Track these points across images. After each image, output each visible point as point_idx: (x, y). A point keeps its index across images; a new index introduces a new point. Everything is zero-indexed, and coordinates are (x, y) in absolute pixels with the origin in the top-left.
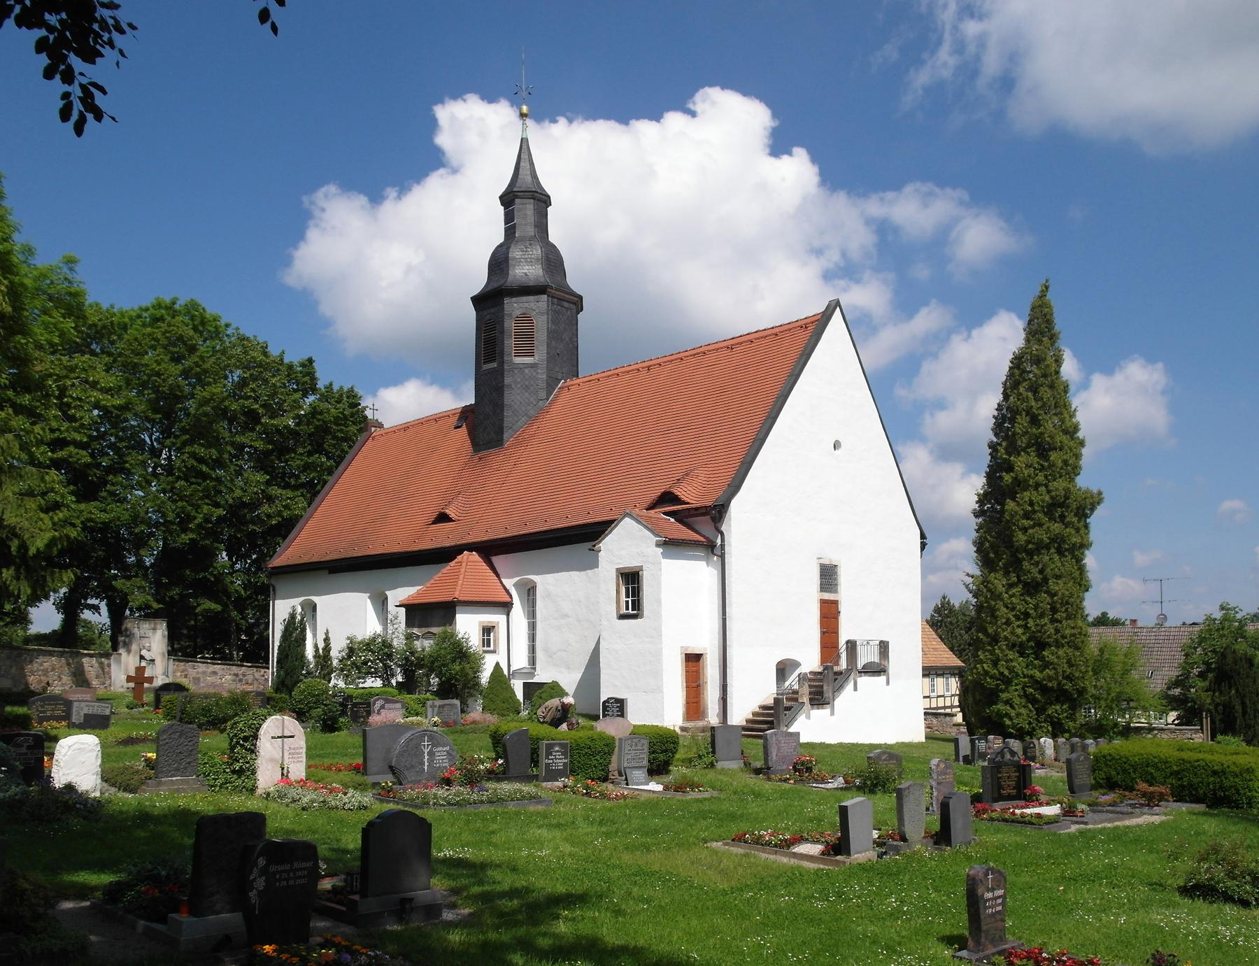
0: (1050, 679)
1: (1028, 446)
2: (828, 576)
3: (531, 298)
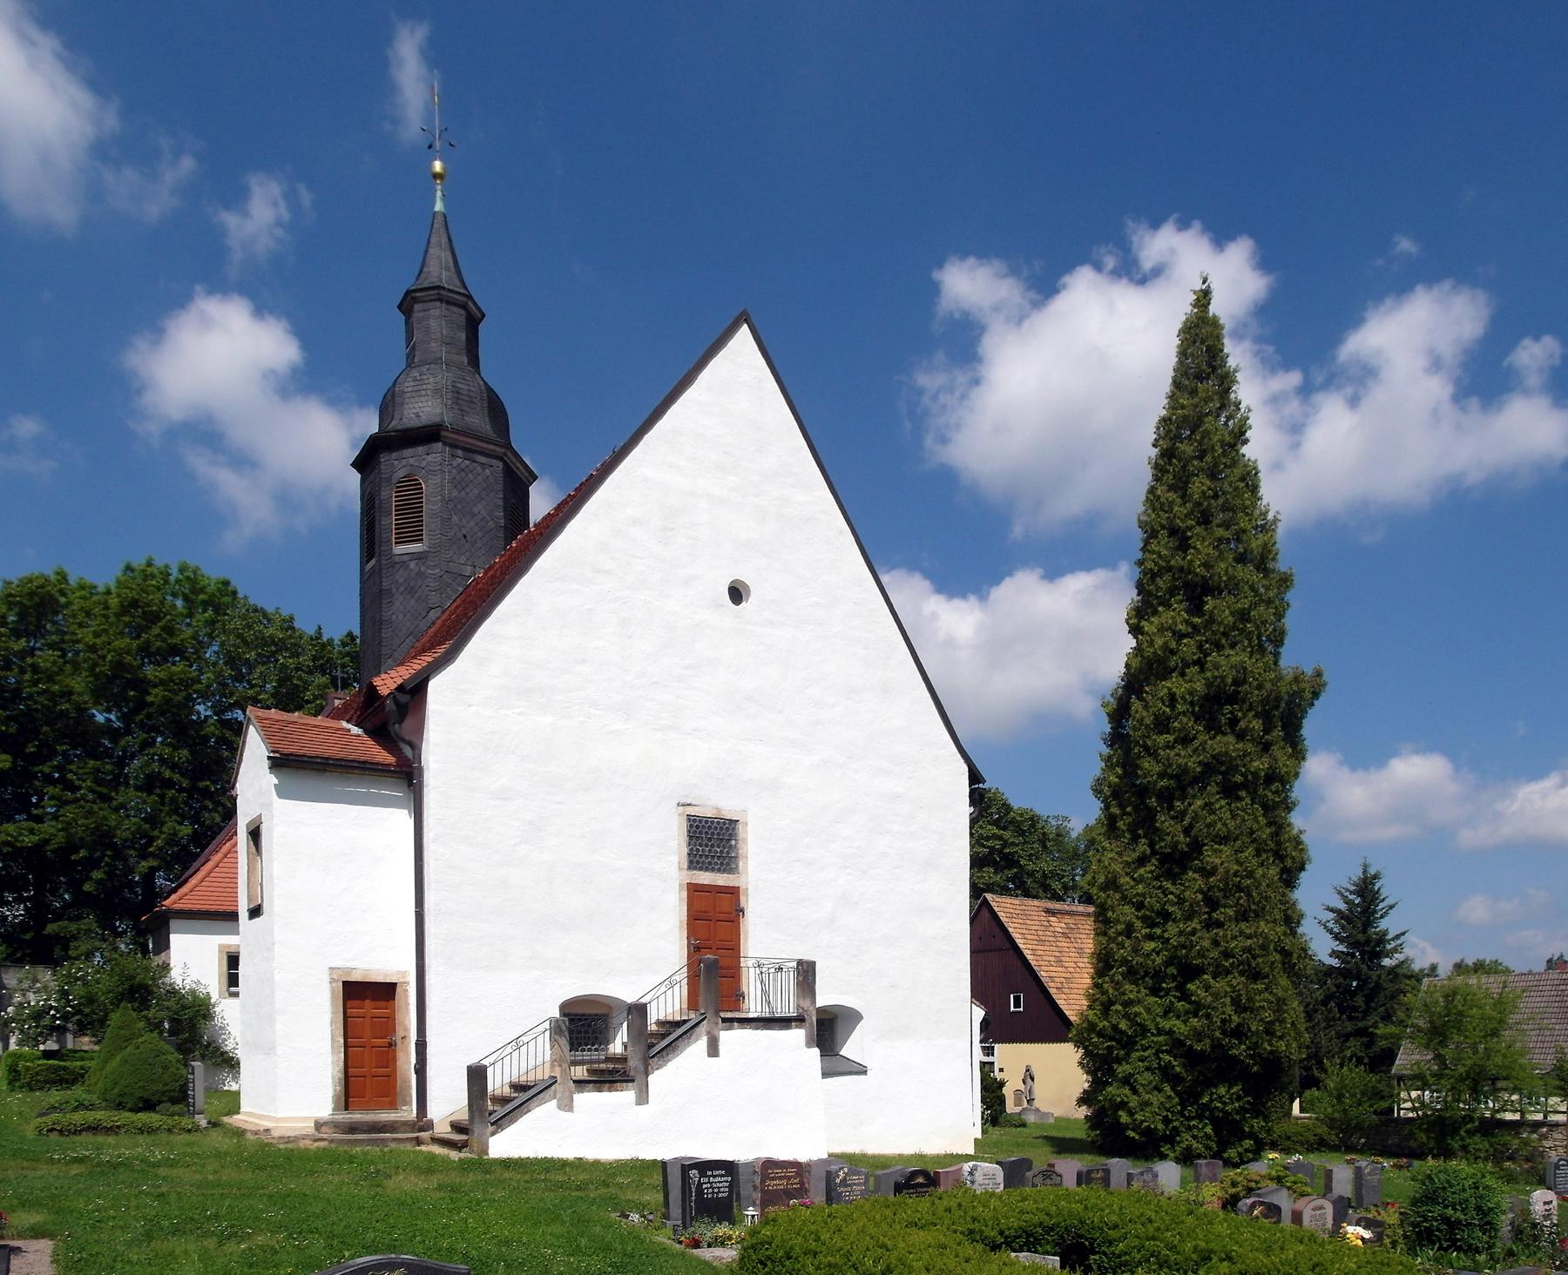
0: (1198, 1035)
1: (1172, 592)
2: (712, 840)
3: (420, 449)
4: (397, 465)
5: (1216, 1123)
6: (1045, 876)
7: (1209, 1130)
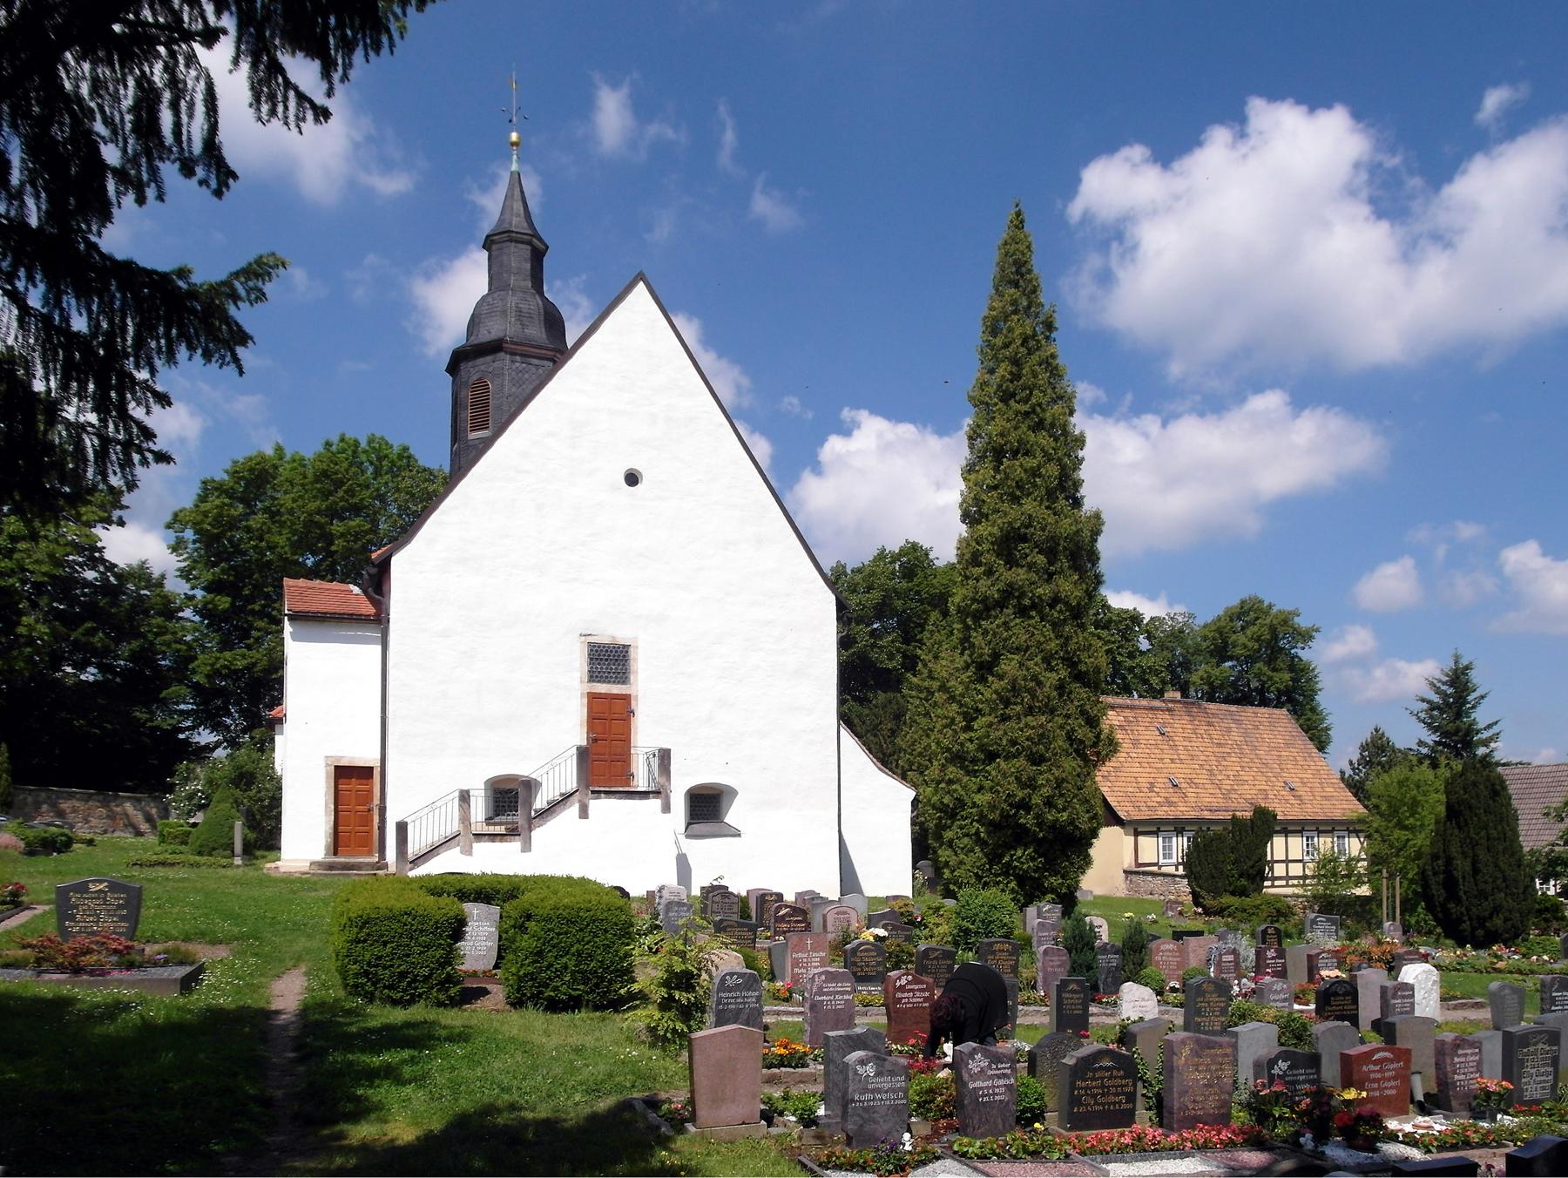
2: (609, 661)
3: (489, 358)
4: (473, 370)
5: (1021, 883)
6: (1144, 672)
7: (1013, 885)
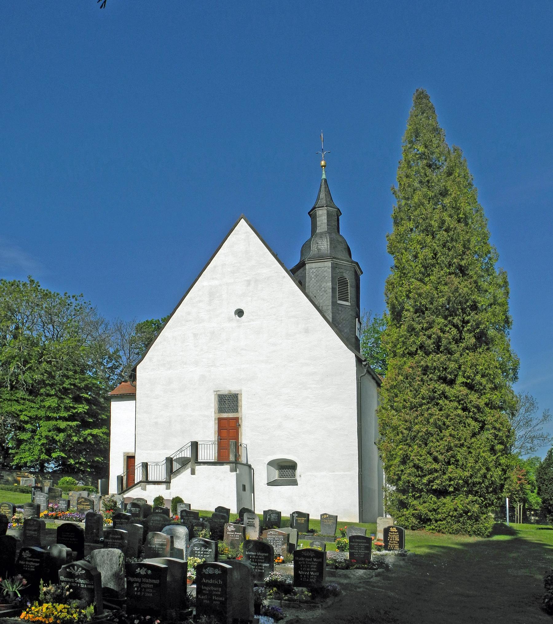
2: (228, 402)
